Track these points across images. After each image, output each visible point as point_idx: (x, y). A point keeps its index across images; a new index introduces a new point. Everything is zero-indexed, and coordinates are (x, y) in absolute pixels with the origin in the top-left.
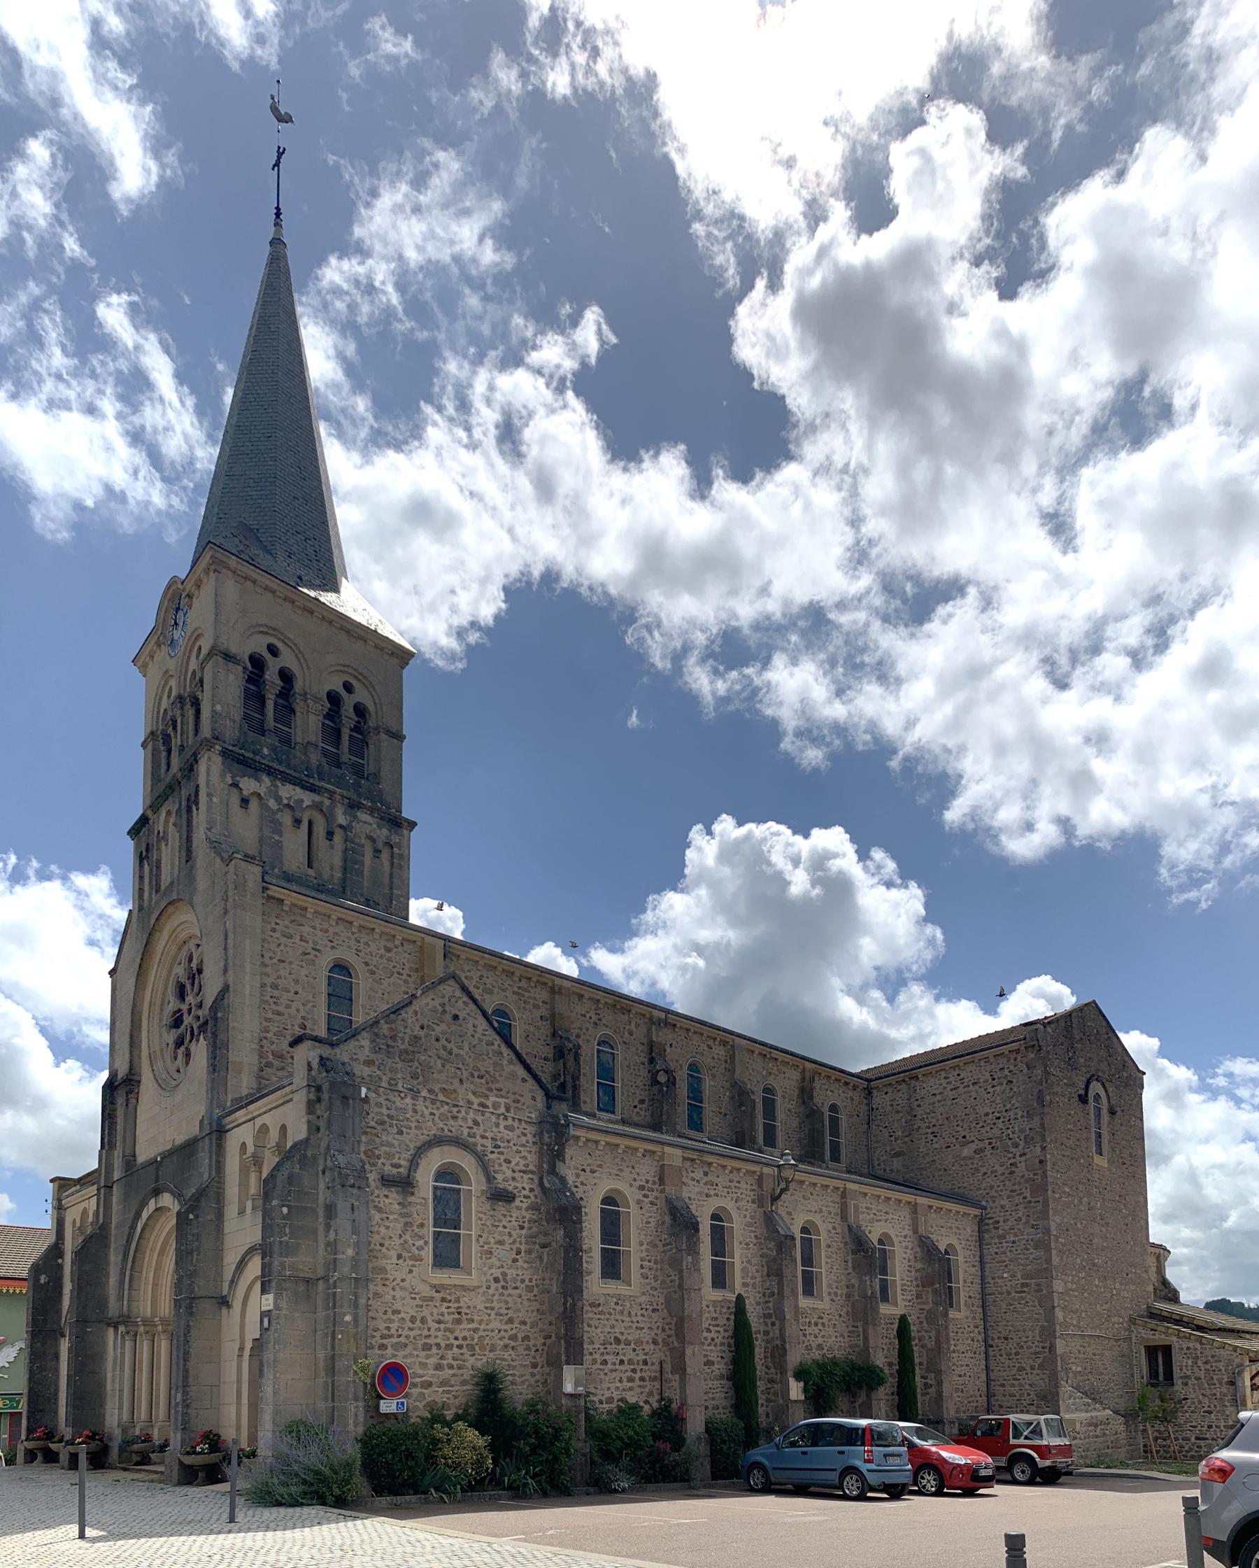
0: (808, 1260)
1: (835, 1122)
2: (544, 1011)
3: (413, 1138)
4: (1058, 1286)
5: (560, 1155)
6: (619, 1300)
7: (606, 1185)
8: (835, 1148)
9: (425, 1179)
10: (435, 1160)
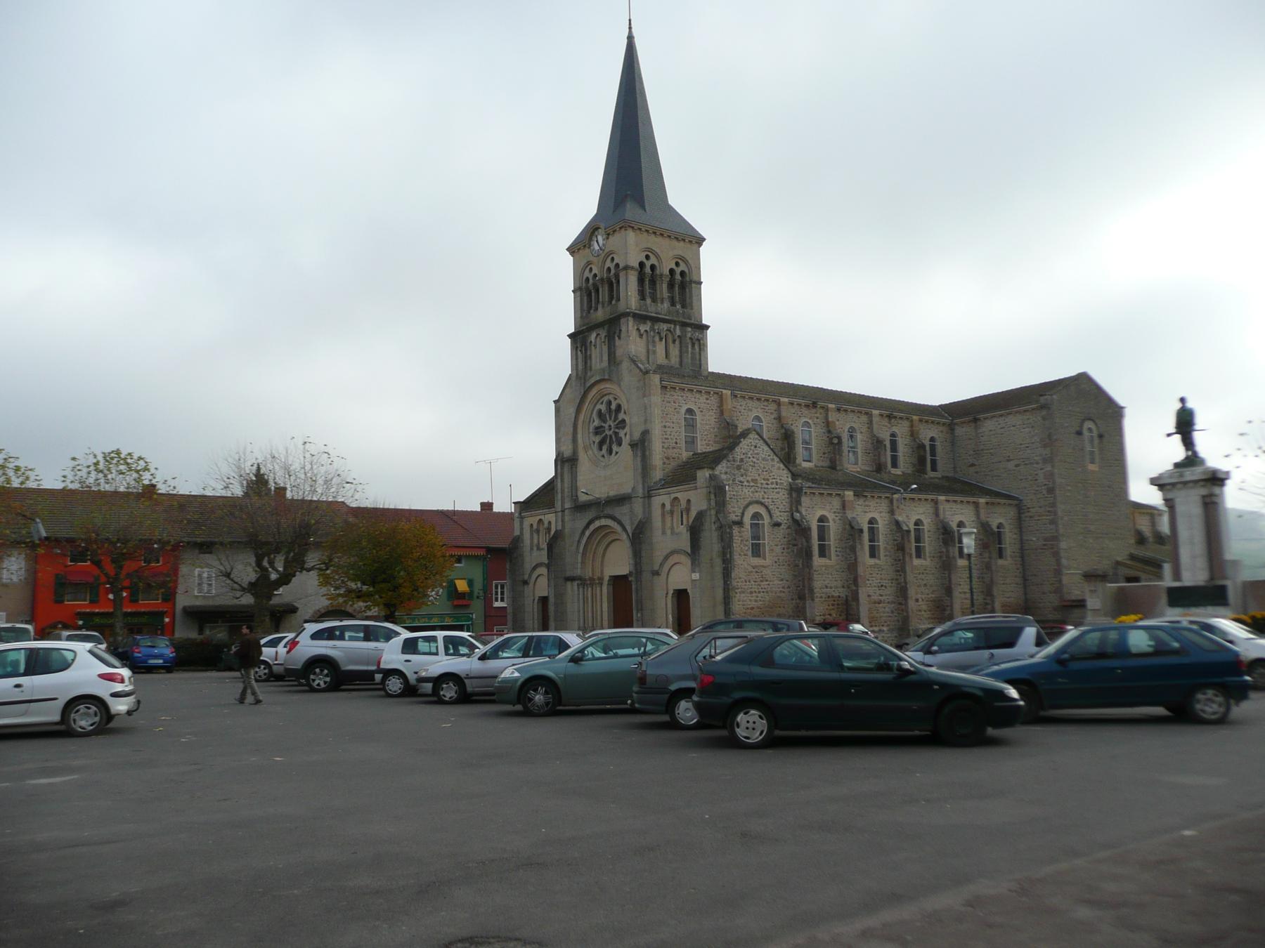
0: (918, 540)
1: (933, 448)
2: (775, 415)
3: (743, 503)
4: (1063, 545)
5: (799, 502)
6: (827, 567)
7: (819, 513)
8: (934, 463)
9: (747, 520)
10: (751, 510)
